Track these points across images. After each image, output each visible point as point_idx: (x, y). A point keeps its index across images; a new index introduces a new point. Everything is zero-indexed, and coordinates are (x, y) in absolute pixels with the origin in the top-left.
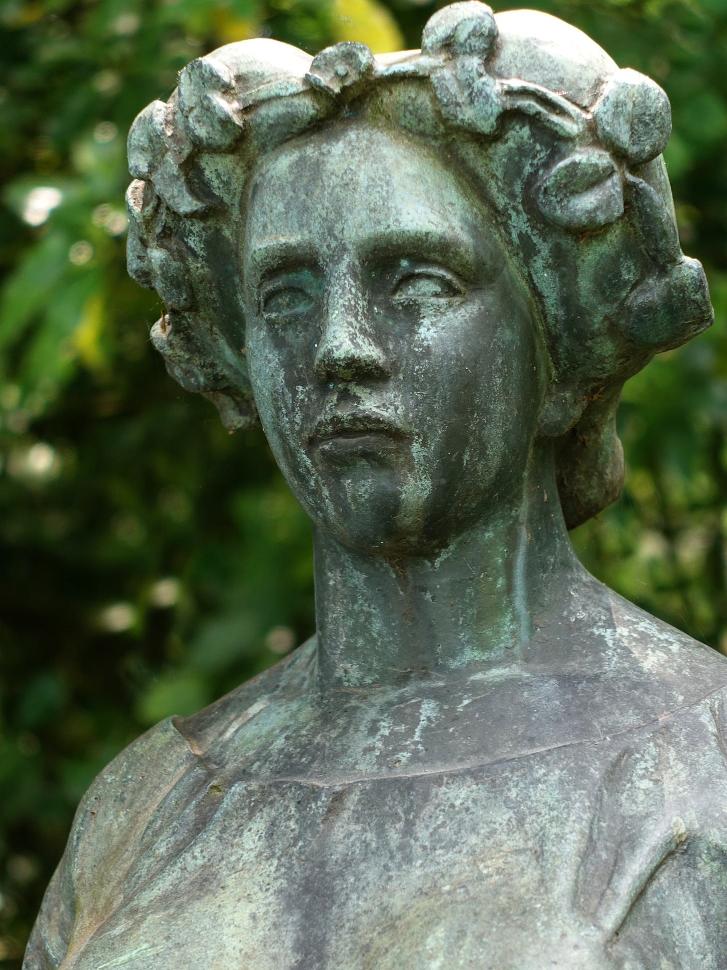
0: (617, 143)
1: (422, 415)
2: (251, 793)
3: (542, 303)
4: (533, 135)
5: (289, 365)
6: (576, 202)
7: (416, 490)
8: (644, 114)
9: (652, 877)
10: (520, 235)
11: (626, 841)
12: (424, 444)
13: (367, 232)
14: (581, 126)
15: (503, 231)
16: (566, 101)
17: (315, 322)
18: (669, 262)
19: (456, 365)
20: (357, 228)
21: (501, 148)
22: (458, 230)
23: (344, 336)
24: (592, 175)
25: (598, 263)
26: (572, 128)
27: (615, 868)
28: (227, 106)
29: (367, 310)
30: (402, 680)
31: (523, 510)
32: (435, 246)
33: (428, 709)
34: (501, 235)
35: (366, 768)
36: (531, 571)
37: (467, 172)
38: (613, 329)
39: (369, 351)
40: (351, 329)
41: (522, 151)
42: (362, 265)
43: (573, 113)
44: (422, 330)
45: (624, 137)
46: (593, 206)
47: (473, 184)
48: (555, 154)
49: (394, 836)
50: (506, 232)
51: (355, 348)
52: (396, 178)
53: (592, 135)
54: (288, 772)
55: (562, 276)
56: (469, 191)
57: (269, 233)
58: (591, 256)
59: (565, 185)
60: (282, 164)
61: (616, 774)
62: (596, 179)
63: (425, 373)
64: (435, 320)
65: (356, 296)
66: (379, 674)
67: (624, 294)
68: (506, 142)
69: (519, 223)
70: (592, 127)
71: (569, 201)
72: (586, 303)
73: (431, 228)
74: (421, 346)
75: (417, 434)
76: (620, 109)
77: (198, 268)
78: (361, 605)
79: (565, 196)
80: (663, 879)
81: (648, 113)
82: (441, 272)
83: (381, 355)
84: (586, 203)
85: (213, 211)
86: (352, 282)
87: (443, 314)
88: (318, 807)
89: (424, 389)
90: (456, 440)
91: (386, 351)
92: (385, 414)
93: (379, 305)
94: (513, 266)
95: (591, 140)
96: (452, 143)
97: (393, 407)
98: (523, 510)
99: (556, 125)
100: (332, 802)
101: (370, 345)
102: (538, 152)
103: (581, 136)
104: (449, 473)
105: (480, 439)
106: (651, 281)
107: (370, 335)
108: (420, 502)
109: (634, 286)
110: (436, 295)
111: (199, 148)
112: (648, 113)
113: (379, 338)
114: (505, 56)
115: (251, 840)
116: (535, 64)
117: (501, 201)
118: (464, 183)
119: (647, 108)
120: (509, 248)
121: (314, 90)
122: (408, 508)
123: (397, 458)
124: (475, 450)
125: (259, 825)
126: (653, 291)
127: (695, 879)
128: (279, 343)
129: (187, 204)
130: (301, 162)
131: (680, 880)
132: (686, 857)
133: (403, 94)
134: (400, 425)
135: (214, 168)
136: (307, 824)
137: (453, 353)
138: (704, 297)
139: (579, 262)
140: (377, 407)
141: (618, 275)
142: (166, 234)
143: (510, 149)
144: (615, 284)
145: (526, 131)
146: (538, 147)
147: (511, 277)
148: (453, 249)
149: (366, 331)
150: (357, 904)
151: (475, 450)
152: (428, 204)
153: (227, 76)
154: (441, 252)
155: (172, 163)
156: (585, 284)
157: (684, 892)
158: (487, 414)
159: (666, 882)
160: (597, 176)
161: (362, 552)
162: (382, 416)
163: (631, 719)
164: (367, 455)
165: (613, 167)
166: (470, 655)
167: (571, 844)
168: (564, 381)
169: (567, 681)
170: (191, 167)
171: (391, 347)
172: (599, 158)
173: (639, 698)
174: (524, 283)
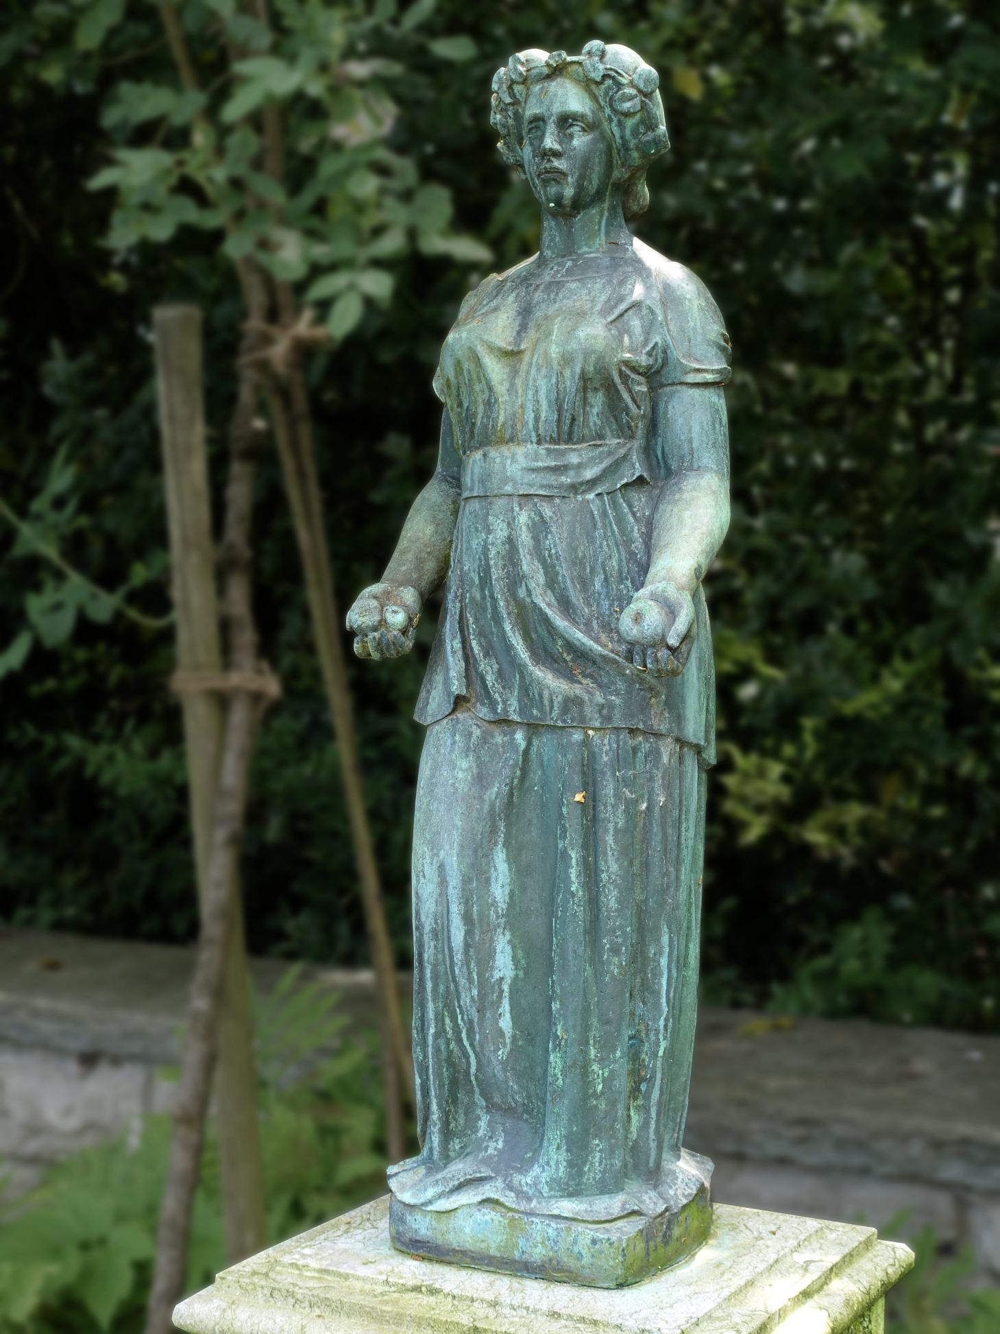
5: (534, 151)
7: (569, 192)
9: (626, 311)
11: (621, 299)
13: (559, 110)
17: (542, 138)
20: (557, 109)
21: (603, 87)
23: (550, 142)
26: (624, 81)
27: (616, 306)
28: (522, 69)
30: (564, 256)
31: (606, 205)
33: (569, 264)
35: (548, 279)
36: (607, 225)
38: (637, 148)
39: (557, 147)
41: (609, 88)
45: (642, 86)
47: (594, 98)
48: (619, 89)
49: (552, 296)
52: (570, 94)
54: (524, 280)
57: (531, 110)
58: (630, 123)
60: (537, 88)
61: (622, 283)
62: (631, 98)
69: (608, 111)
70: (631, 81)
77: (511, 122)
78: (553, 232)
80: (630, 312)
84: (627, 105)
85: (516, 103)
88: (531, 288)
90: (582, 177)
94: (606, 124)
96: (588, 84)
98: (606, 205)
104: (580, 188)
111: (513, 82)
114: (607, 58)
115: (511, 298)
116: (616, 61)
117: (603, 103)
121: (548, 65)
125: (514, 294)
126: (650, 136)
128: (531, 144)
129: (508, 100)
130: (542, 88)
133: (575, 67)
135: (518, 89)
136: (528, 293)
142: (502, 110)
150: (539, 314)
153: (523, 59)
155: (505, 87)
156: (628, 132)
161: (554, 214)
163: (630, 269)
164: (555, 180)
166: (585, 249)
167: (603, 298)
168: (623, 165)
169: (613, 259)
170: (510, 88)
172: (633, 91)
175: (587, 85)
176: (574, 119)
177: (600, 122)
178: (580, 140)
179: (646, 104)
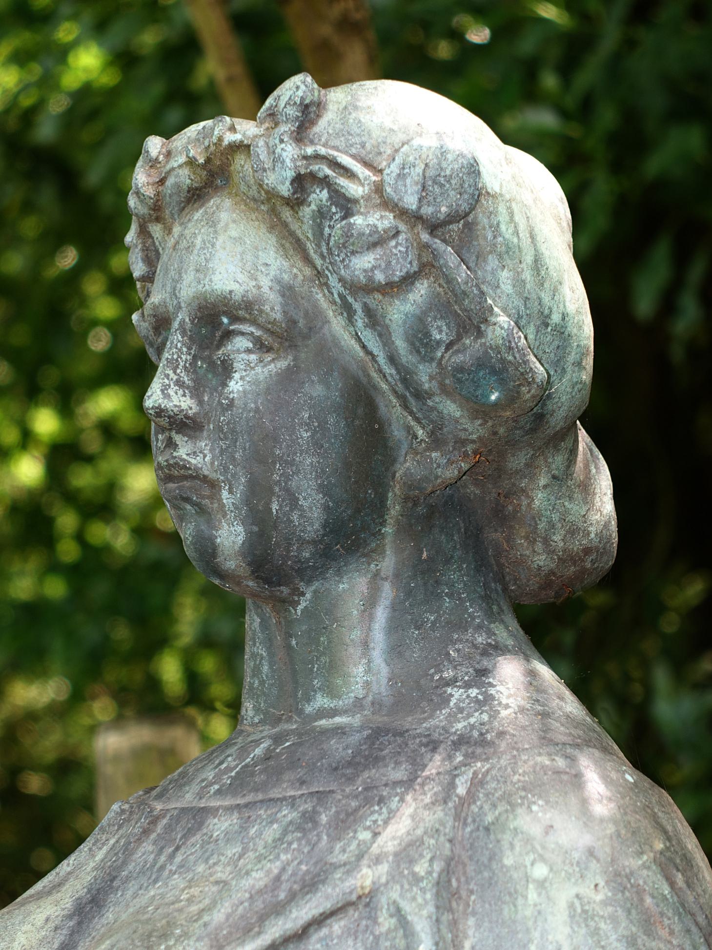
0: (400, 204)
1: (226, 463)
2: (123, 811)
3: (376, 362)
4: (330, 198)
6: (356, 261)
8: (439, 175)
10: (339, 295)
12: (231, 491)
14: (367, 188)
15: (326, 291)
16: (354, 162)
18: (481, 323)
19: (254, 416)
22: (265, 289)
24: (370, 235)
25: (405, 322)
26: (354, 190)
27: (278, 909)
29: (190, 364)
31: (388, 563)
32: (240, 304)
34: (324, 295)
37: (291, 235)
40: (166, 381)
42: (192, 322)
43: (361, 176)
44: (232, 384)
46: (370, 265)
50: (329, 292)
51: (164, 398)
53: (380, 197)
55: (380, 335)
56: (291, 252)
58: (399, 312)
59: (344, 244)
63: (228, 424)
64: (244, 374)
65: (180, 350)
66: (264, 714)
67: (439, 354)
68: (310, 205)
71: (350, 261)
72: (407, 362)
73: (234, 287)
74: (228, 398)
75: (223, 482)
76: (407, 171)
79: (347, 255)
80: (337, 926)
81: (443, 174)
82: (252, 329)
83: (193, 406)
86: (180, 338)
87: (253, 368)
89: (226, 438)
90: (257, 494)
91: (200, 403)
92: (193, 461)
93: (203, 359)
95: (378, 202)
97: (202, 455)
98: (388, 563)
99: (342, 187)
100: (148, 824)
101: (184, 395)
102: (334, 214)
103: (367, 198)
105: (287, 490)
106: (468, 342)
107: (188, 387)
108: (236, 548)
109: (449, 346)
110: (248, 351)
112: (443, 174)
113: (196, 390)
118: (287, 245)
119: (442, 169)
120: (334, 307)
122: (226, 553)
123: (212, 503)
124: (283, 501)
127: (372, 933)
131: (356, 931)
132: (368, 910)
134: (206, 473)
137: (253, 405)
138: (515, 358)
139: (387, 321)
140: (188, 455)
141: (428, 335)
143: (313, 211)
144: (427, 343)
145: (325, 194)
146: (334, 210)
147: (333, 336)
148: (257, 307)
149: (184, 383)
151: (283, 501)
152: (240, 264)
154: (247, 310)
156: (400, 344)
157: (355, 944)
158: (292, 465)
159: (339, 932)
160: (376, 236)
162: (189, 462)
165: (397, 228)
171: (206, 398)
173: (422, 754)
174: (353, 342)
175: (273, 211)
176: (235, 319)
177: (315, 318)
178: (249, 374)
179: (435, 255)
